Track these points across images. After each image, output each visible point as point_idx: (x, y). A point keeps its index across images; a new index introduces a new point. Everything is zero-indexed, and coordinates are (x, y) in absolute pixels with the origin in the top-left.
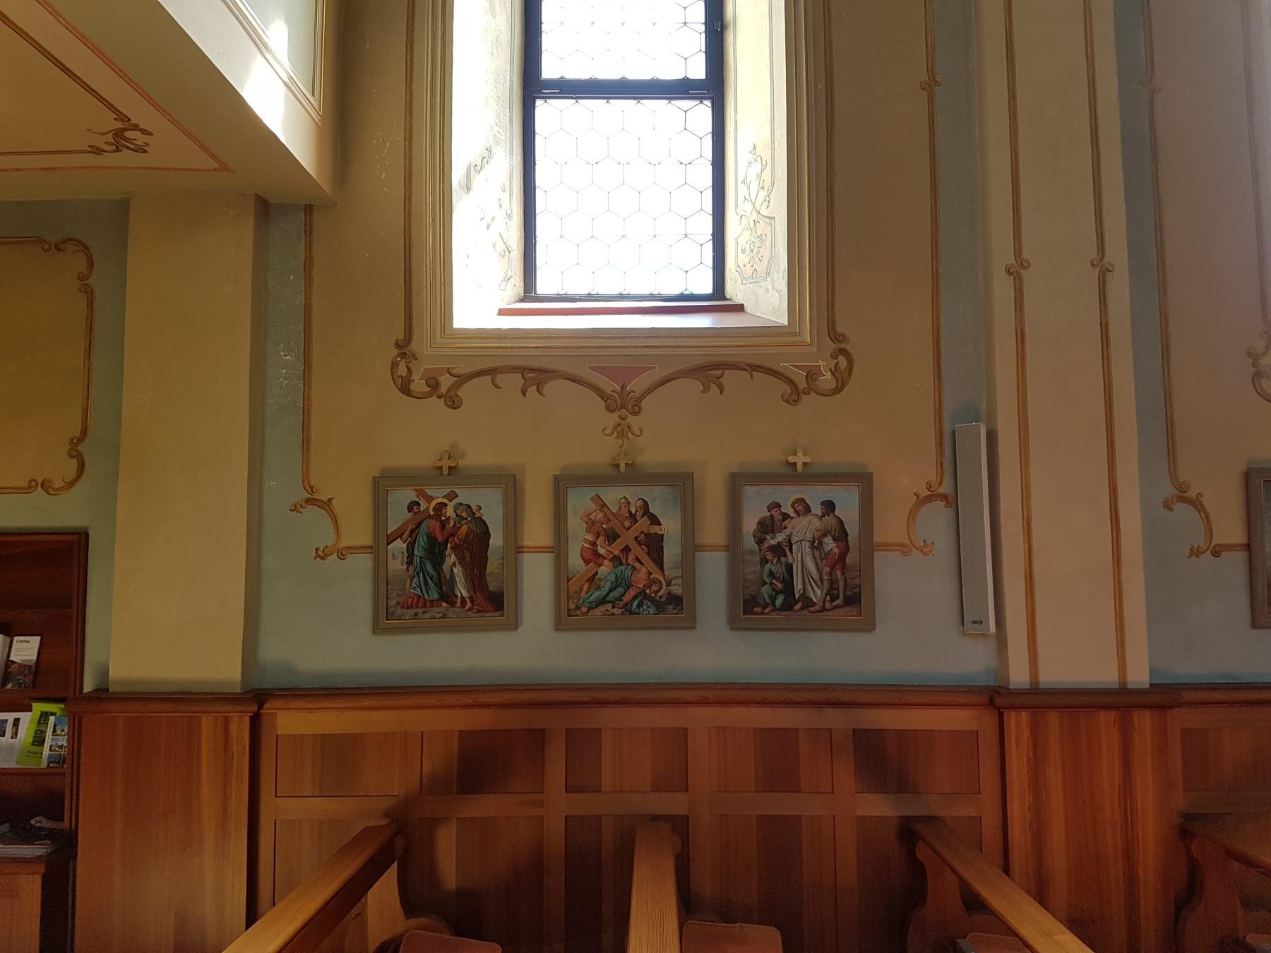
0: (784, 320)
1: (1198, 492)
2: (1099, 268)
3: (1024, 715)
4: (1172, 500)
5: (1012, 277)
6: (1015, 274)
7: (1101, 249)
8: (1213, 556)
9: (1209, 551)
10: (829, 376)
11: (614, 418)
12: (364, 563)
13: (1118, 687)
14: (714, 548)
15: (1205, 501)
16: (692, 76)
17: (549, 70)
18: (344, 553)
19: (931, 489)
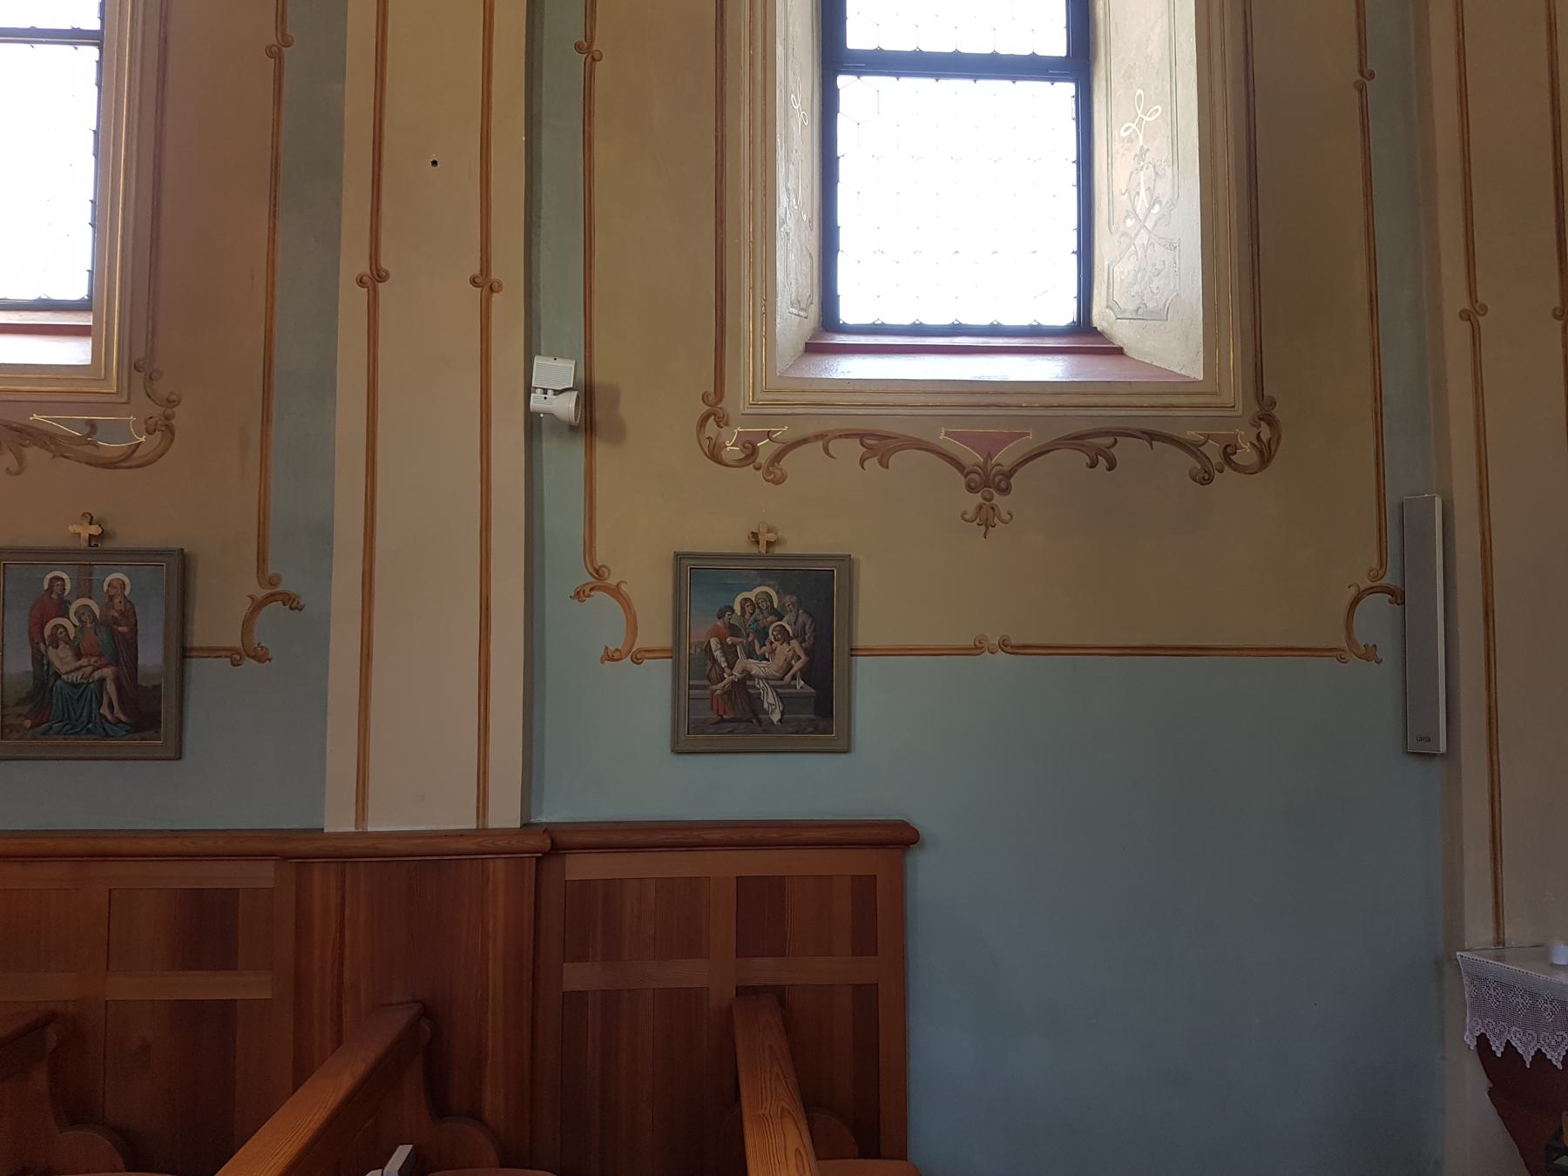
0: (1199, 375)
10: (1247, 447)
11: (977, 498)
13: (474, 826)
17: (858, 37)
18: (639, 656)
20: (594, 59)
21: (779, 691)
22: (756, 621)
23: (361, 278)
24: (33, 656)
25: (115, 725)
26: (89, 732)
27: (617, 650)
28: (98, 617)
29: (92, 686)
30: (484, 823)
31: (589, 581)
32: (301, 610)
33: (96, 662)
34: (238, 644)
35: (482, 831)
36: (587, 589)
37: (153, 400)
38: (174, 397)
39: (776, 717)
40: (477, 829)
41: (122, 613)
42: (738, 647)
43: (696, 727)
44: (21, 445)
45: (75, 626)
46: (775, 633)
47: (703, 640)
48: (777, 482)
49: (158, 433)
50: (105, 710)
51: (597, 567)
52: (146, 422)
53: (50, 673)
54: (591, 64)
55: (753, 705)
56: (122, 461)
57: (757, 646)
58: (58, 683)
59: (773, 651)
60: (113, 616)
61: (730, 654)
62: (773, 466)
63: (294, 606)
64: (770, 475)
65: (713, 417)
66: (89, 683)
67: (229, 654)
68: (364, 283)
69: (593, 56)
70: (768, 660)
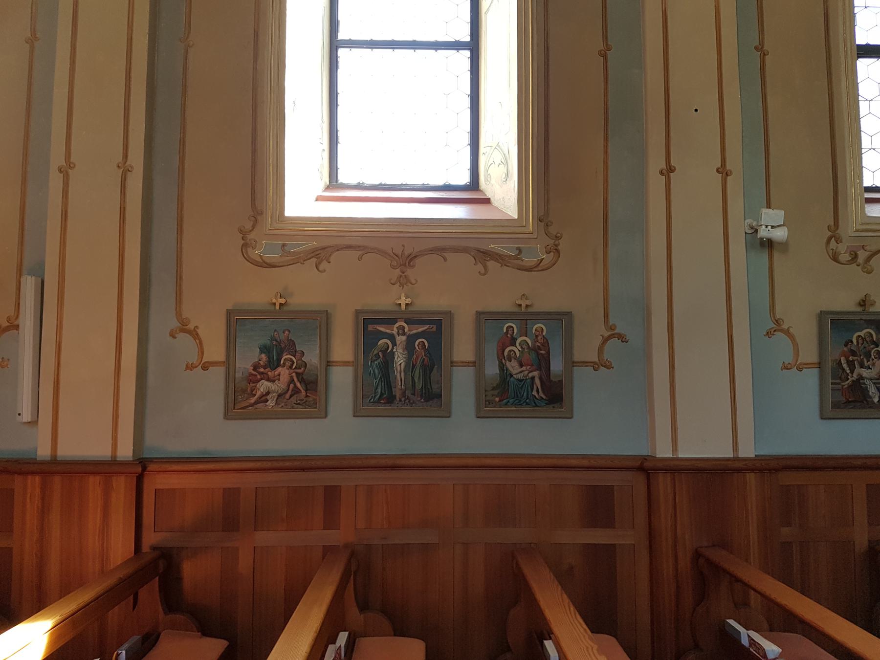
1: (195, 325)
2: (122, 169)
3: (38, 479)
4: (176, 331)
5: (62, 175)
6: (65, 172)
7: (126, 156)
8: (202, 369)
9: (201, 365)
11: (397, 272)
12: (218, 373)
13: (732, 456)
14: (345, 364)
15: (199, 331)
16: (469, 56)
17: (342, 35)
19: (10, 322)
20: (764, 55)
21: (878, 385)
22: (865, 348)
23: (662, 171)
24: (499, 366)
25: (540, 400)
26: (527, 404)
27: (789, 364)
28: (530, 346)
29: (528, 380)
30: (737, 454)
31: (773, 327)
32: (627, 342)
33: (530, 368)
34: (597, 360)
35: (736, 459)
36: (772, 331)
37: (549, 237)
38: (558, 235)
39: (876, 400)
40: (734, 457)
41: (542, 344)
42: (856, 362)
43: (836, 405)
44: (485, 260)
45: (519, 351)
46: (875, 354)
47: (837, 358)
48: (869, 272)
49: (552, 254)
50: (535, 393)
51: (777, 319)
52: (545, 247)
53: (508, 374)
54: (763, 57)
55: (865, 391)
56: (534, 267)
57: (865, 360)
58: (512, 379)
59: (874, 364)
60: (538, 346)
61: (851, 364)
62: (866, 264)
63: (623, 340)
64: (865, 269)
65: (833, 239)
66: (526, 379)
67: (592, 364)
68: (664, 174)
69: (764, 53)
70: (871, 369)
